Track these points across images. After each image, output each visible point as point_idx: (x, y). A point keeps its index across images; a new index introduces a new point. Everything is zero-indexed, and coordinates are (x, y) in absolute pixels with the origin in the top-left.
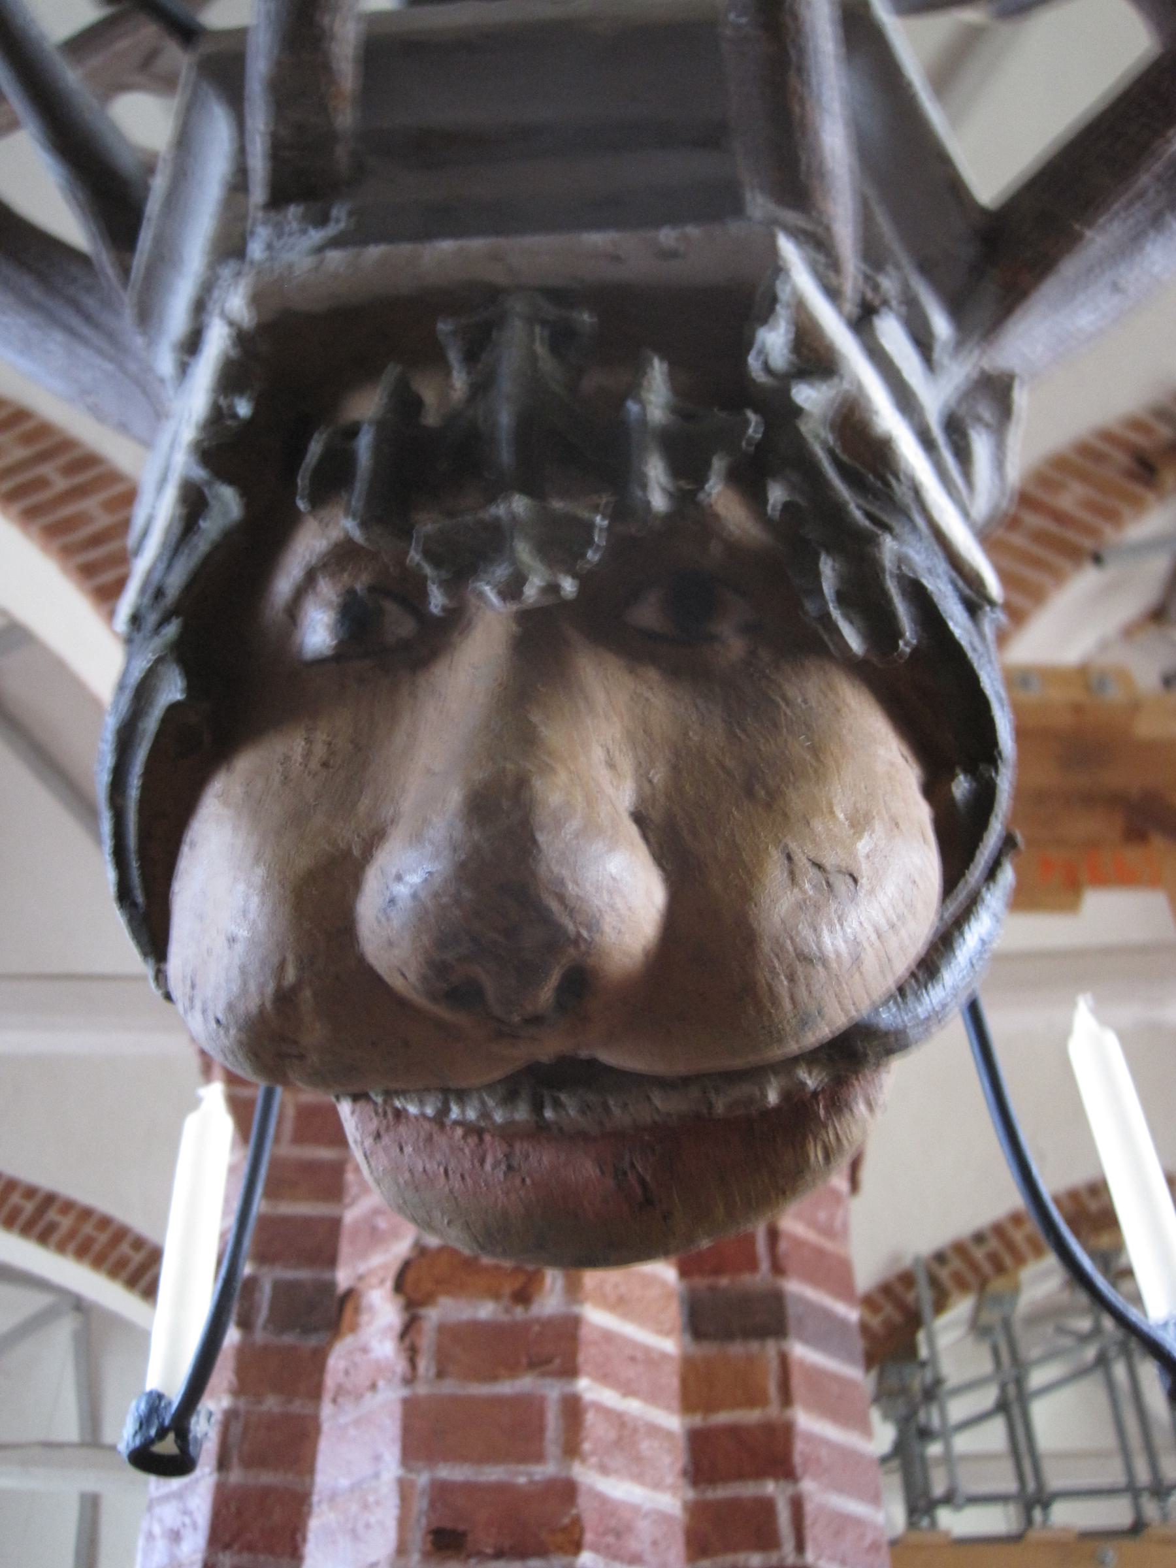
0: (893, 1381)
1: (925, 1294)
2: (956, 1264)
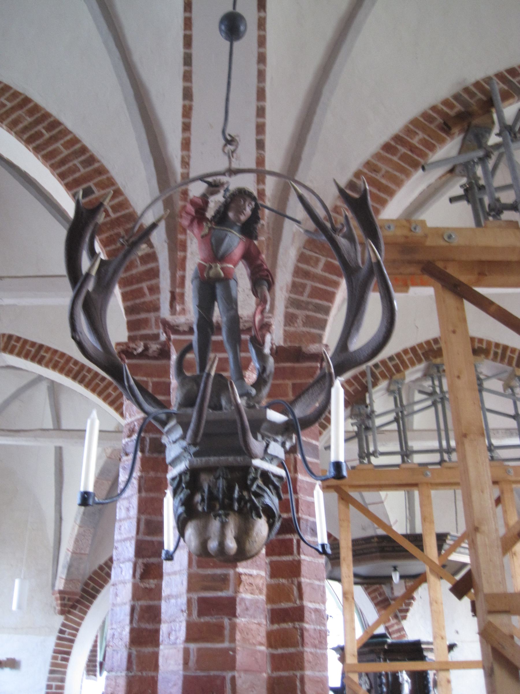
0: (356, 410)
1: (370, 379)
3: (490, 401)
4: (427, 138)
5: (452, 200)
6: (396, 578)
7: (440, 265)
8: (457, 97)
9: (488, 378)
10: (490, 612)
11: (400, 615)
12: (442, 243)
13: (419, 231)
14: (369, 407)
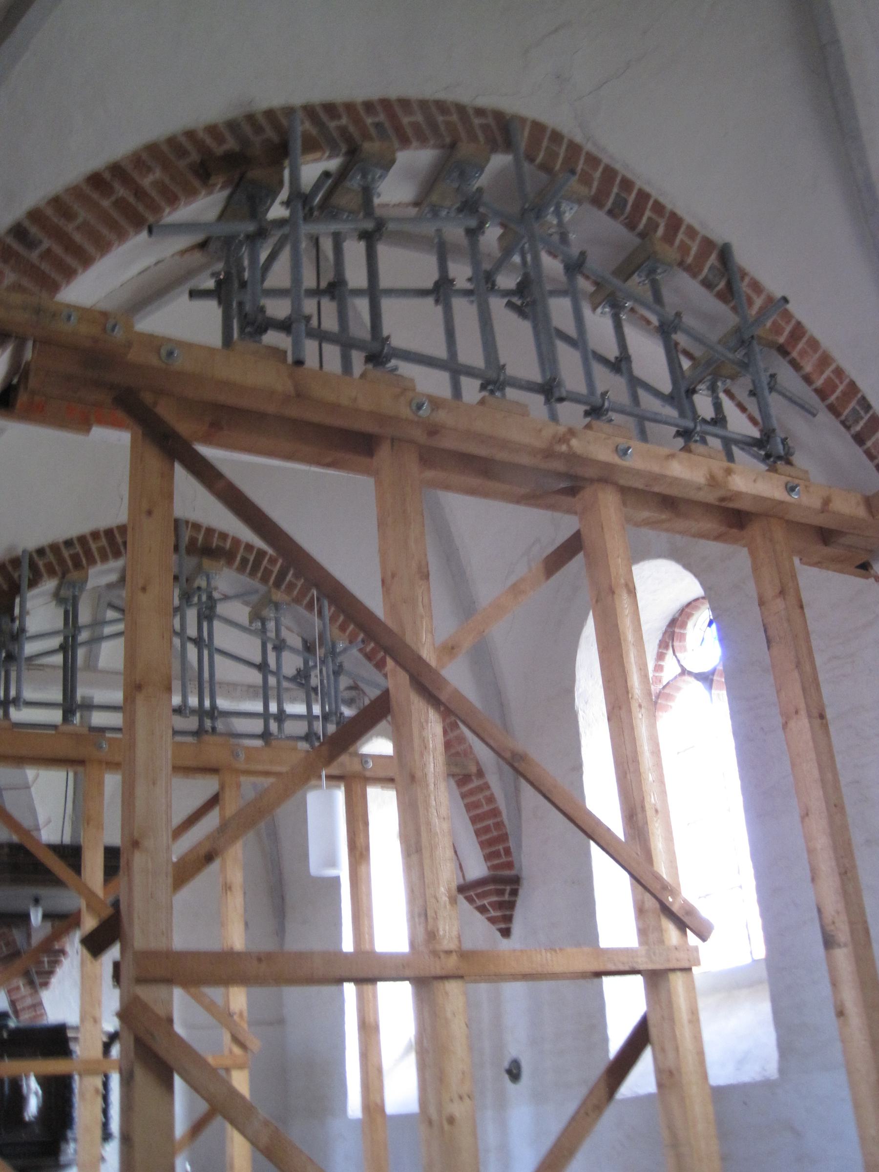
2: (51, 557)
3: (224, 636)
4: (167, 181)
5: (194, 294)
6: (36, 917)
7: (148, 397)
8: (232, 125)
9: (226, 598)
10: (141, 980)
11: (37, 980)
12: (154, 361)
13: (119, 334)
14: (17, 622)
